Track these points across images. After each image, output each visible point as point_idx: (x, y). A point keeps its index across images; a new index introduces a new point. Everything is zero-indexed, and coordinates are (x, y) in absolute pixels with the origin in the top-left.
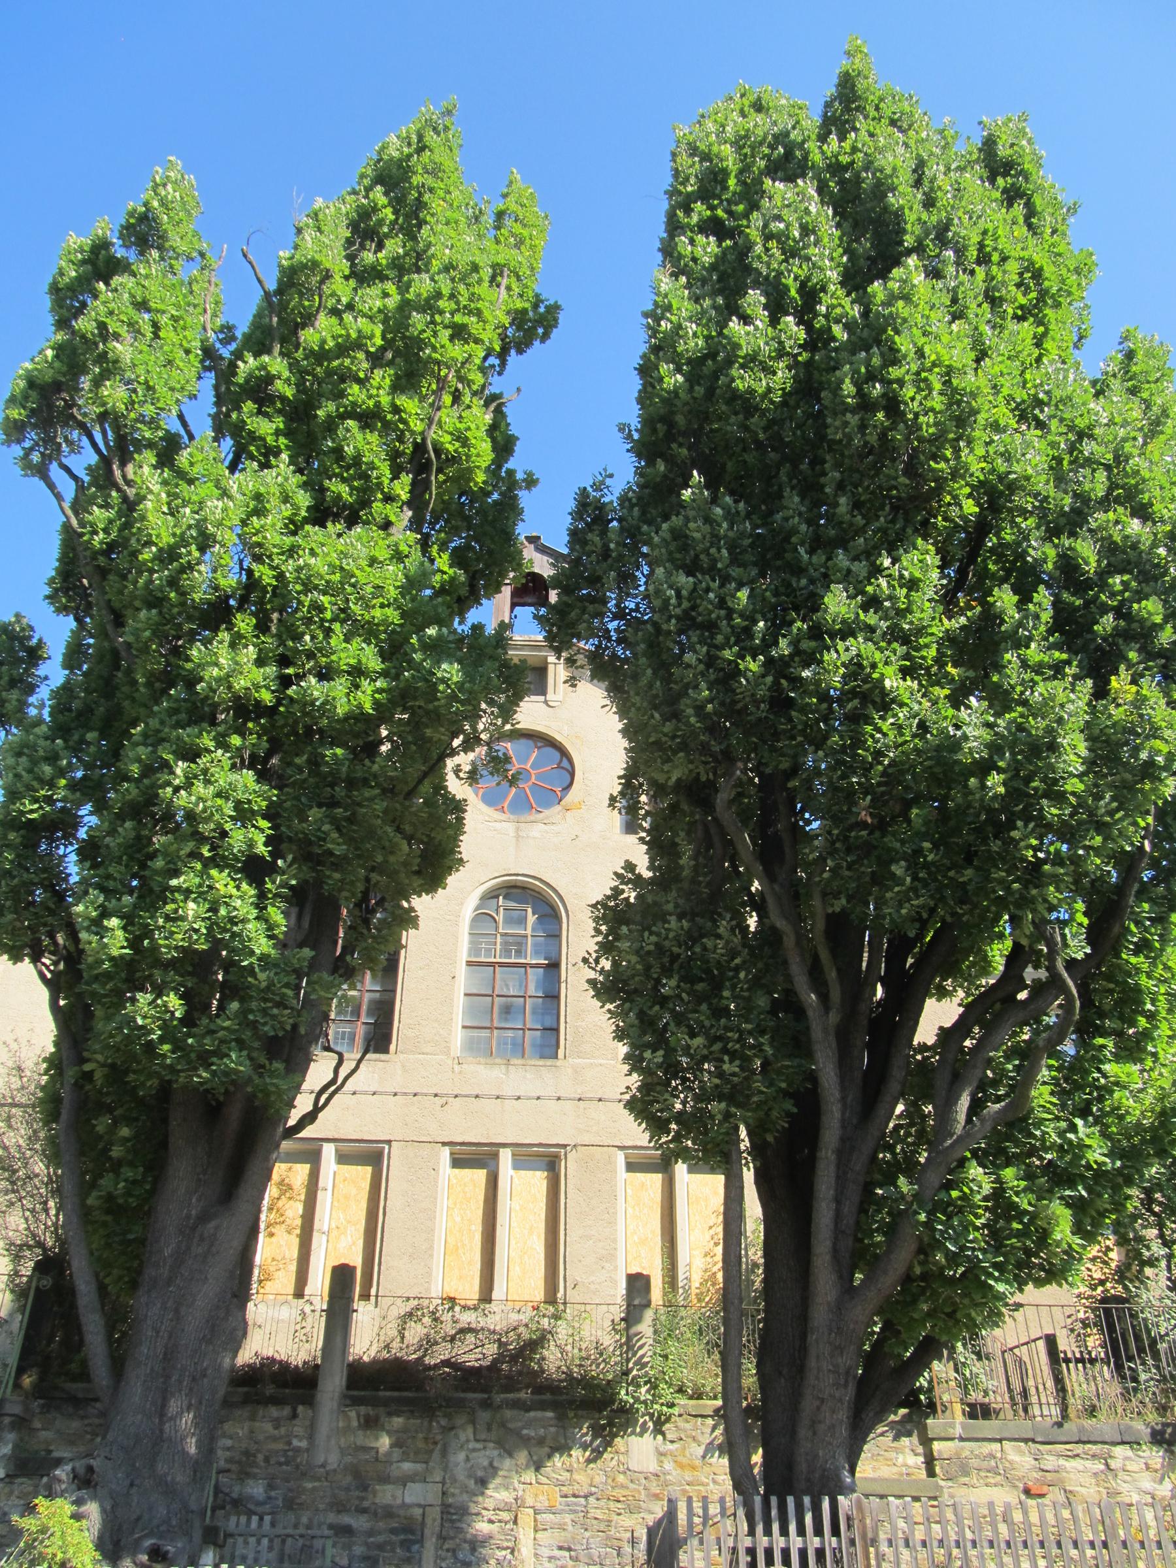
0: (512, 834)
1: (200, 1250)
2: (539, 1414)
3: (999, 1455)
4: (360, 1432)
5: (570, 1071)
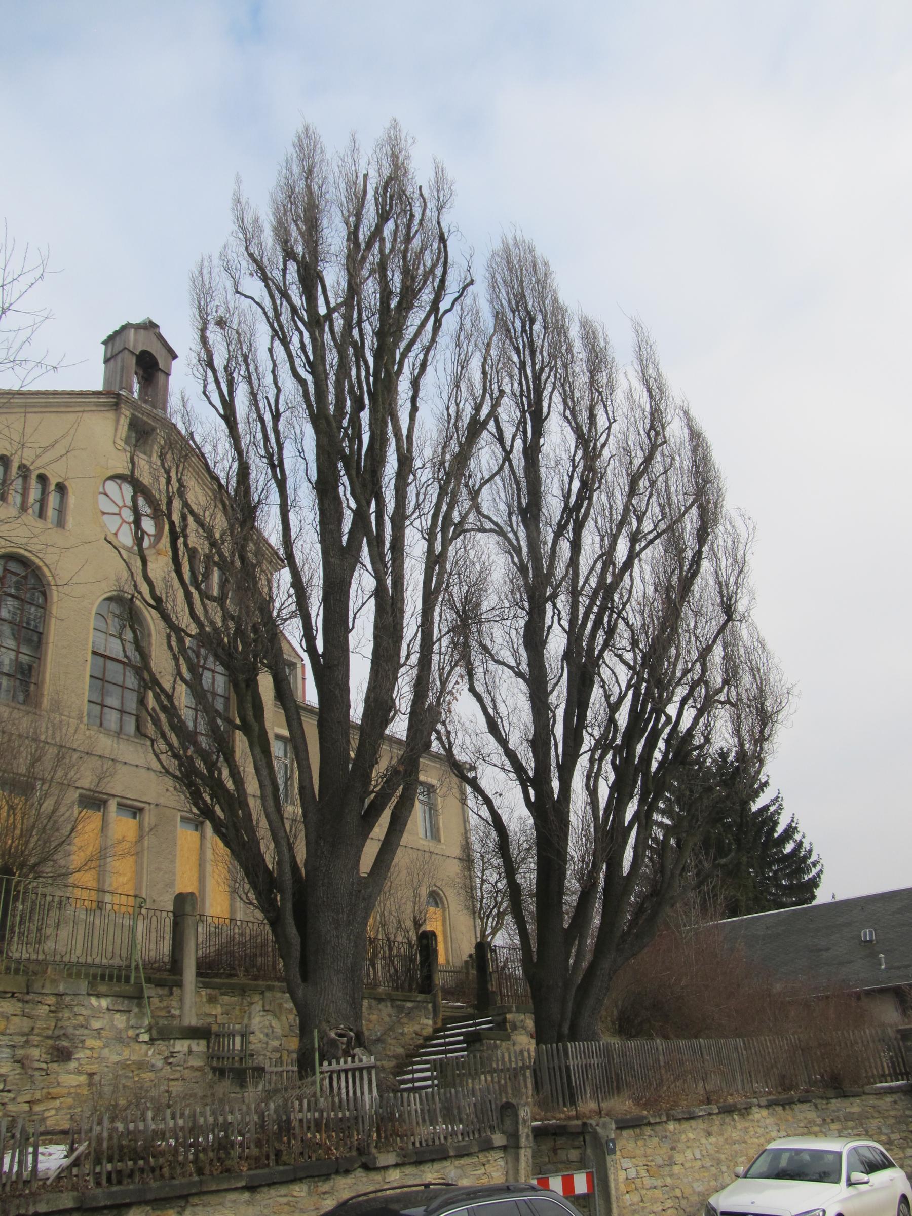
4: (207, 1005)
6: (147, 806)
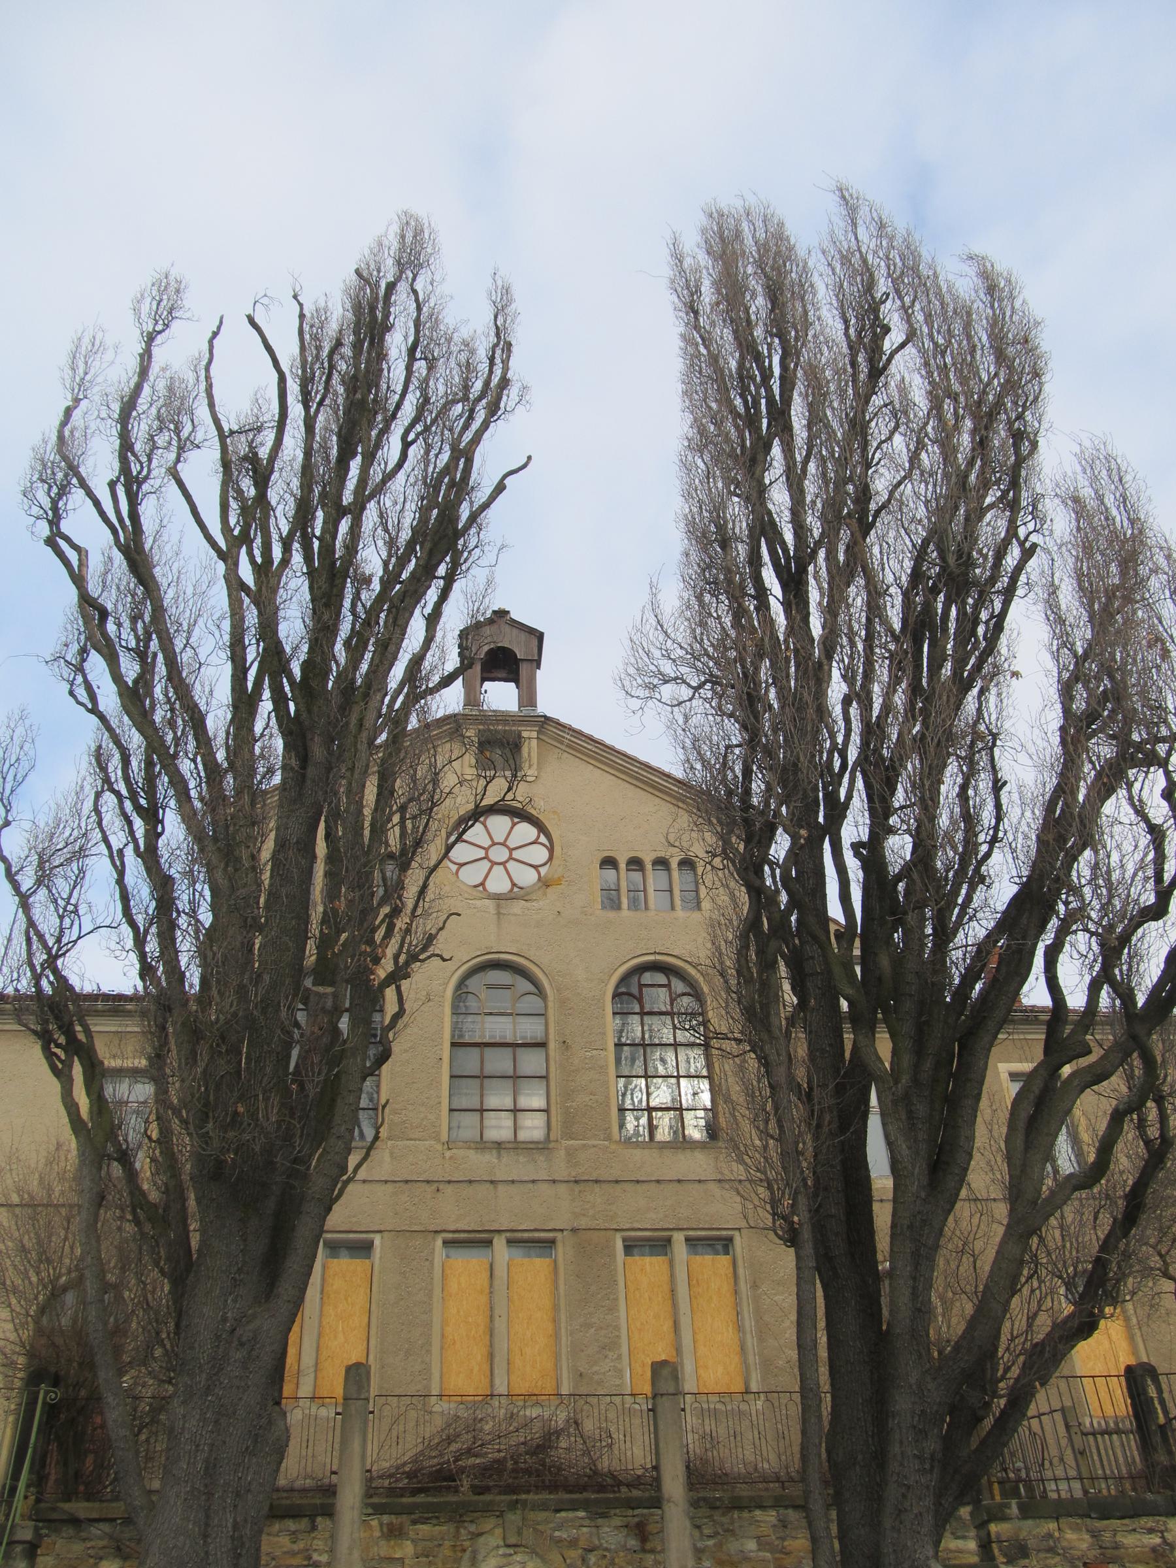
0: (492, 910)
1: (239, 1355)
2: (571, 1514)
3: (1057, 1534)
4: (383, 1543)
5: (562, 1153)
6: (559, 1235)
